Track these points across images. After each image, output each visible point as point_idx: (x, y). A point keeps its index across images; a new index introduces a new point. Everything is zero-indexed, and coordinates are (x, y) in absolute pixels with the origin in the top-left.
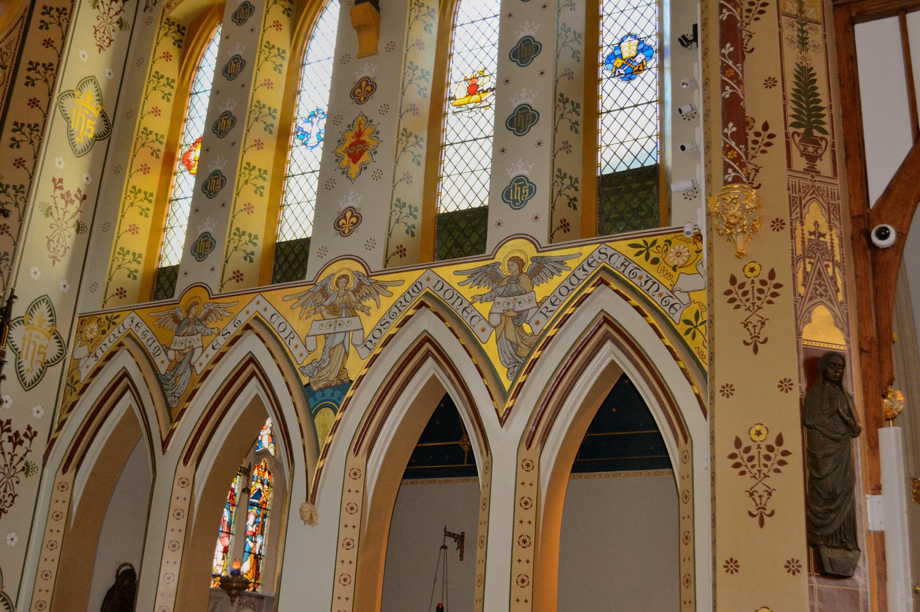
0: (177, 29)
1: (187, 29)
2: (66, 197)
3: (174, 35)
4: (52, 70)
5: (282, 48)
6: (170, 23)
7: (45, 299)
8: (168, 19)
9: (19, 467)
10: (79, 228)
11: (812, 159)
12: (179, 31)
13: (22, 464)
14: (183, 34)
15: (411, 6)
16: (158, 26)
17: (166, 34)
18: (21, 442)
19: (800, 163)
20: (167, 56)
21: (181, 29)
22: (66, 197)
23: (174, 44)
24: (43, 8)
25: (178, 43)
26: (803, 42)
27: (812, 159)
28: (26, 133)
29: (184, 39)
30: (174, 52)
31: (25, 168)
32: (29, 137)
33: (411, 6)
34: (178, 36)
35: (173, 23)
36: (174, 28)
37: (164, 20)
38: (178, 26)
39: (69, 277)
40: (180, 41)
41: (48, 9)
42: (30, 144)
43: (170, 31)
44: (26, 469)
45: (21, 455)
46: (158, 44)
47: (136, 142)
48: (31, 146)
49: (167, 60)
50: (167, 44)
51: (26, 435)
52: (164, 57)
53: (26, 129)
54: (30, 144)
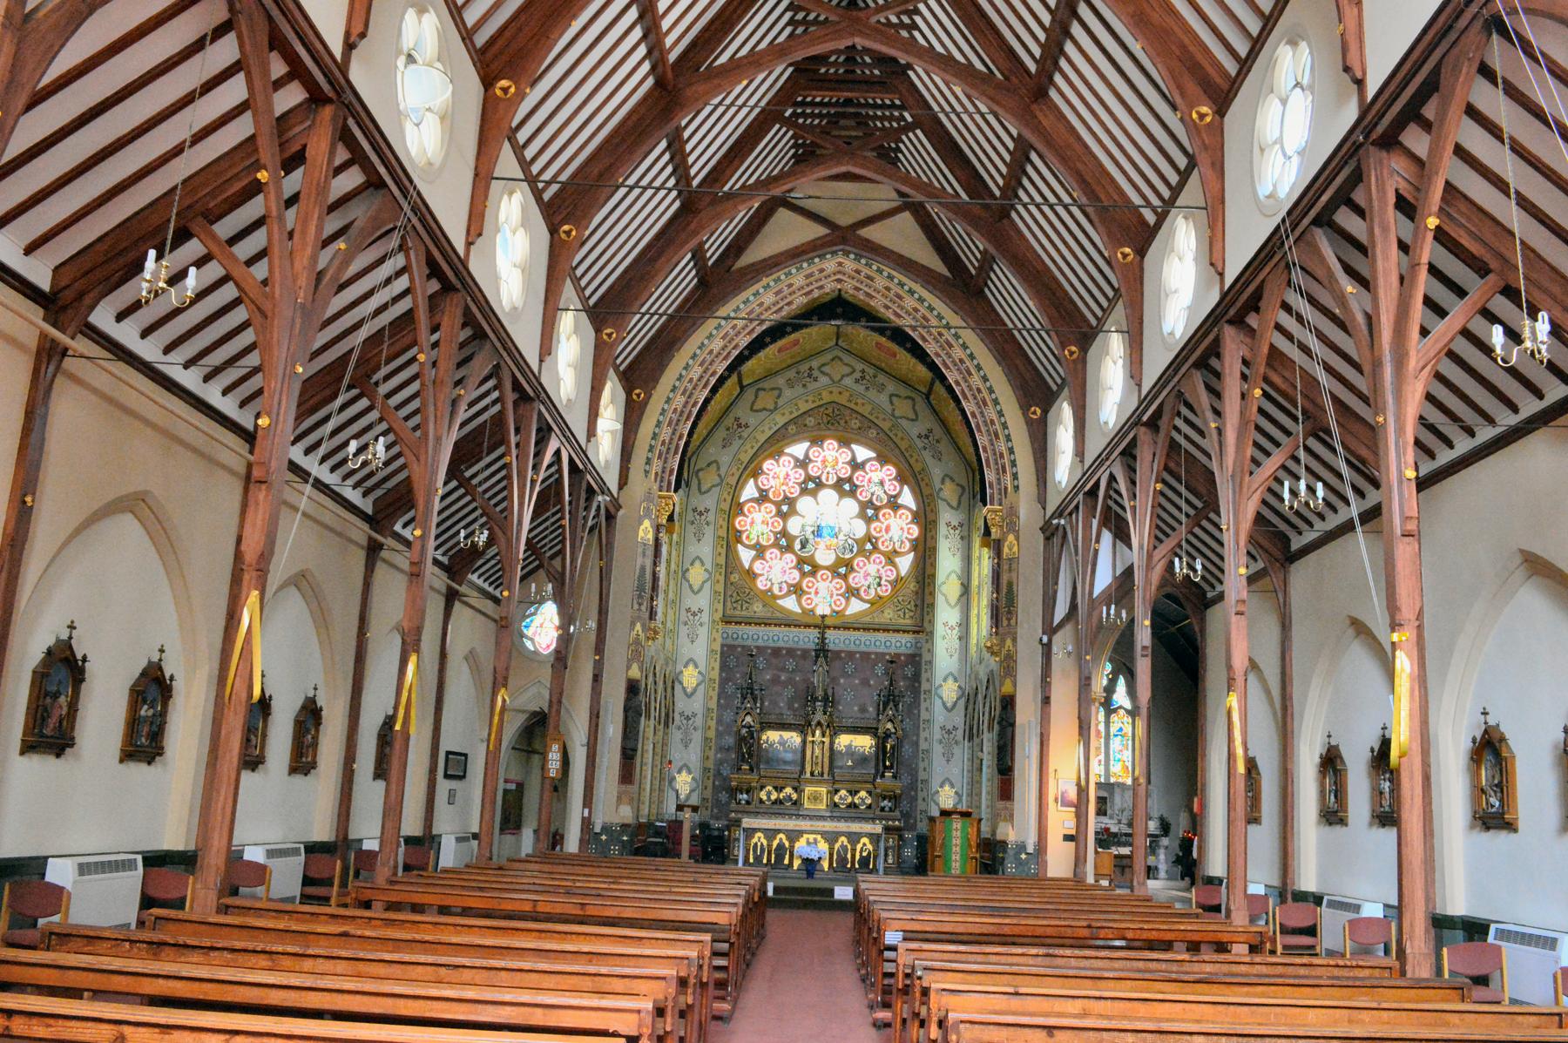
2: (952, 628)
4: (932, 633)
7: (951, 674)
10: (960, 638)
11: (640, 604)
19: (636, 607)
22: (952, 628)
26: (644, 555)
27: (640, 604)
39: (960, 660)
44: (956, 743)
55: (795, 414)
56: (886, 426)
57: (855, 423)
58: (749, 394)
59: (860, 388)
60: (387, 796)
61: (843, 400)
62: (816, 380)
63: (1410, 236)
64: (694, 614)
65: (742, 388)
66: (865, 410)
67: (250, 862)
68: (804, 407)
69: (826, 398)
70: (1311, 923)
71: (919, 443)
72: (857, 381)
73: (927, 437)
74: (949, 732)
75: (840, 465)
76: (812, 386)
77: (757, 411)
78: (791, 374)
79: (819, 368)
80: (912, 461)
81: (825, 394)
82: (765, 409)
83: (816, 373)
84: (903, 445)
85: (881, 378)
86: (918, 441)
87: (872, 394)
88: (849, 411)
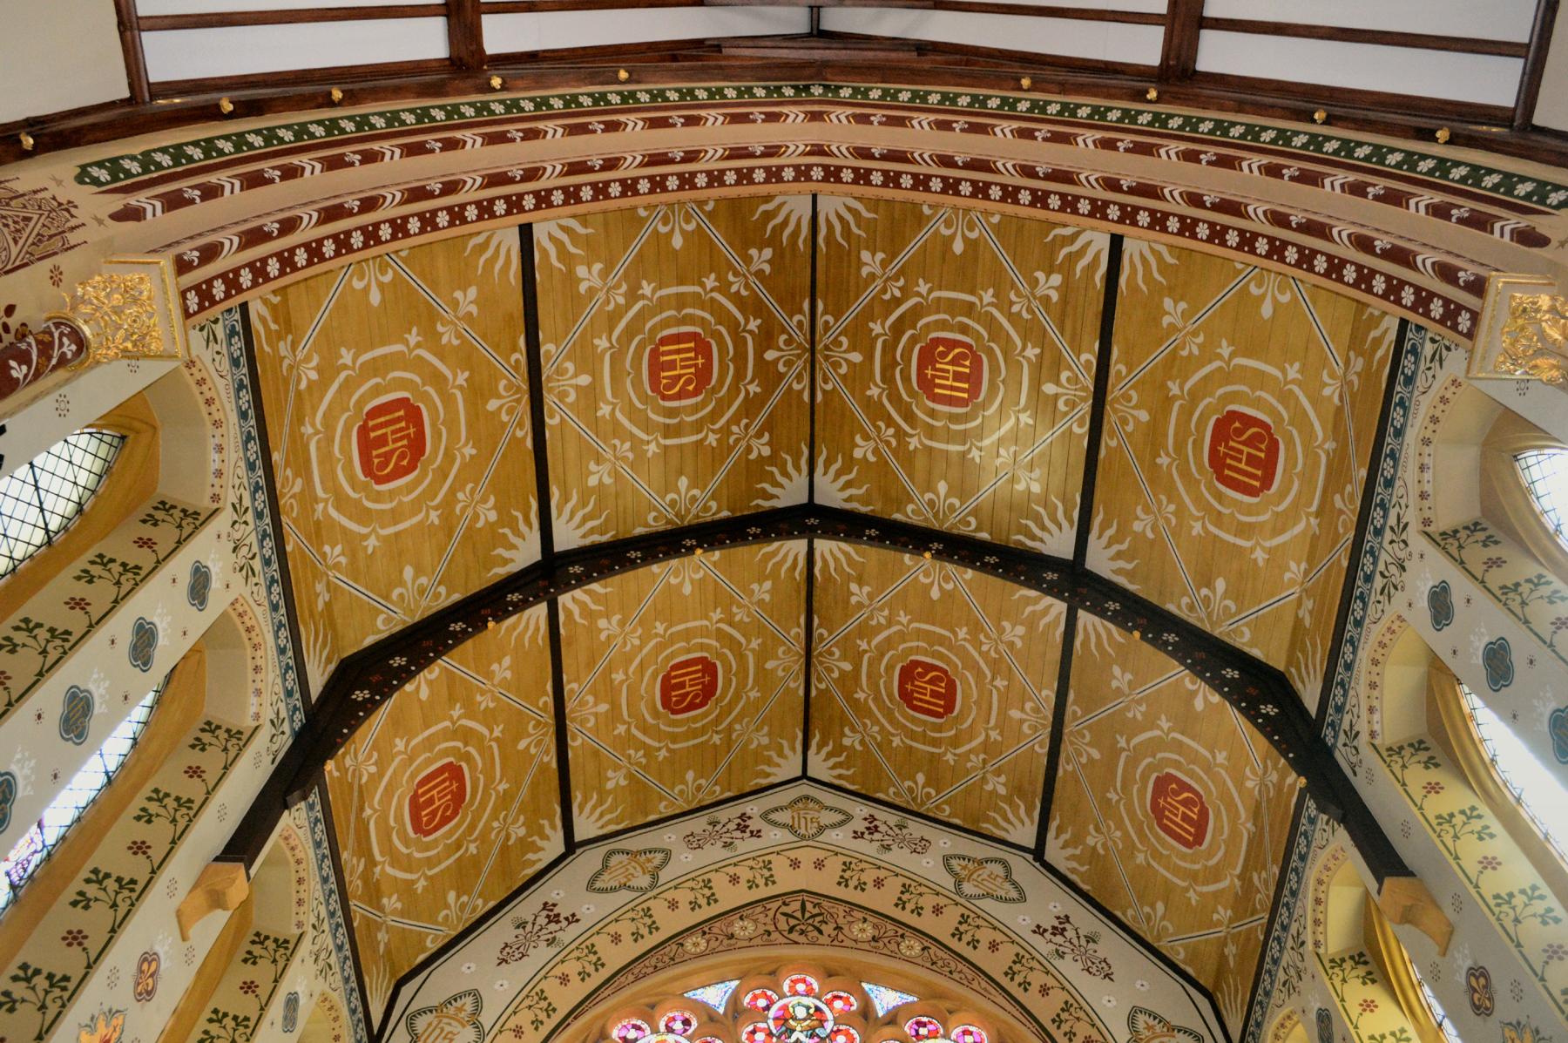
0: (1352, 963)
1: (1366, 952)
3: (1354, 973)
5: (1396, 1029)
6: (1337, 963)
8: (1332, 961)
9: (898, 831)
12: (1357, 963)
13: (896, 829)
14: (1366, 963)
15: (1435, 831)
16: (1326, 978)
17: (1344, 980)
18: (558, 922)
20: (1369, 1006)
21: (1359, 959)
23: (1364, 983)
24: (20, 968)
25: (1369, 978)
28: (228, 1027)
29: (1372, 967)
30: (1374, 992)
31: (84, 949)
32: (41, 997)
33: (1435, 831)
34: (1362, 971)
35: (1343, 960)
36: (1348, 965)
37: (1328, 965)
38: (1352, 958)
40: (1370, 973)
41: (220, 1015)
42: (39, 1009)
43: (1346, 972)
45: (886, 828)
46: (1343, 1000)
47: (1502, 926)
48: (172, 826)
49: (1372, 1011)
50: (1356, 991)
51: (752, 832)
52: (1364, 1010)
53: (963, 928)
54: (39, 1009)
55: (597, 979)
56: (941, 927)
57: (862, 930)
58: (588, 861)
59: (867, 847)
60: (1525, 68)
61: (825, 882)
62: (756, 834)
63: (1211, 980)
64: (555, 919)
65: (572, 846)
66: (884, 900)
67: (1197, 38)
68: (731, 897)
69: (787, 880)
70: (1398, 321)
71: (1043, 945)
72: (858, 835)
73: (1057, 931)
74: (1057, 931)
75: (829, 1026)
76: (746, 845)
77: (601, 890)
78: (698, 824)
79: (765, 816)
80: (1031, 1000)
81: (780, 865)
82: (624, 886)
83: (754, 825)
84: (996, 964)
85: (916, 828)
86: (1037, 941)
87: (900, 857)
88: (840, 910)
